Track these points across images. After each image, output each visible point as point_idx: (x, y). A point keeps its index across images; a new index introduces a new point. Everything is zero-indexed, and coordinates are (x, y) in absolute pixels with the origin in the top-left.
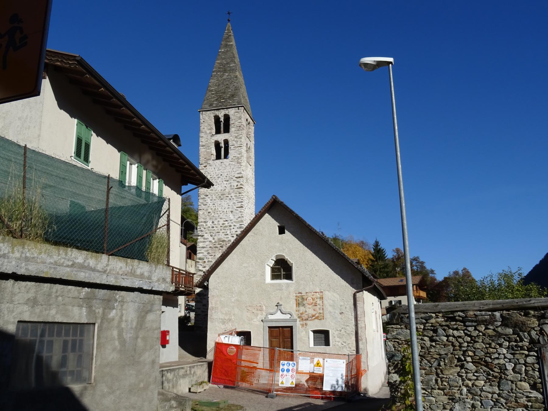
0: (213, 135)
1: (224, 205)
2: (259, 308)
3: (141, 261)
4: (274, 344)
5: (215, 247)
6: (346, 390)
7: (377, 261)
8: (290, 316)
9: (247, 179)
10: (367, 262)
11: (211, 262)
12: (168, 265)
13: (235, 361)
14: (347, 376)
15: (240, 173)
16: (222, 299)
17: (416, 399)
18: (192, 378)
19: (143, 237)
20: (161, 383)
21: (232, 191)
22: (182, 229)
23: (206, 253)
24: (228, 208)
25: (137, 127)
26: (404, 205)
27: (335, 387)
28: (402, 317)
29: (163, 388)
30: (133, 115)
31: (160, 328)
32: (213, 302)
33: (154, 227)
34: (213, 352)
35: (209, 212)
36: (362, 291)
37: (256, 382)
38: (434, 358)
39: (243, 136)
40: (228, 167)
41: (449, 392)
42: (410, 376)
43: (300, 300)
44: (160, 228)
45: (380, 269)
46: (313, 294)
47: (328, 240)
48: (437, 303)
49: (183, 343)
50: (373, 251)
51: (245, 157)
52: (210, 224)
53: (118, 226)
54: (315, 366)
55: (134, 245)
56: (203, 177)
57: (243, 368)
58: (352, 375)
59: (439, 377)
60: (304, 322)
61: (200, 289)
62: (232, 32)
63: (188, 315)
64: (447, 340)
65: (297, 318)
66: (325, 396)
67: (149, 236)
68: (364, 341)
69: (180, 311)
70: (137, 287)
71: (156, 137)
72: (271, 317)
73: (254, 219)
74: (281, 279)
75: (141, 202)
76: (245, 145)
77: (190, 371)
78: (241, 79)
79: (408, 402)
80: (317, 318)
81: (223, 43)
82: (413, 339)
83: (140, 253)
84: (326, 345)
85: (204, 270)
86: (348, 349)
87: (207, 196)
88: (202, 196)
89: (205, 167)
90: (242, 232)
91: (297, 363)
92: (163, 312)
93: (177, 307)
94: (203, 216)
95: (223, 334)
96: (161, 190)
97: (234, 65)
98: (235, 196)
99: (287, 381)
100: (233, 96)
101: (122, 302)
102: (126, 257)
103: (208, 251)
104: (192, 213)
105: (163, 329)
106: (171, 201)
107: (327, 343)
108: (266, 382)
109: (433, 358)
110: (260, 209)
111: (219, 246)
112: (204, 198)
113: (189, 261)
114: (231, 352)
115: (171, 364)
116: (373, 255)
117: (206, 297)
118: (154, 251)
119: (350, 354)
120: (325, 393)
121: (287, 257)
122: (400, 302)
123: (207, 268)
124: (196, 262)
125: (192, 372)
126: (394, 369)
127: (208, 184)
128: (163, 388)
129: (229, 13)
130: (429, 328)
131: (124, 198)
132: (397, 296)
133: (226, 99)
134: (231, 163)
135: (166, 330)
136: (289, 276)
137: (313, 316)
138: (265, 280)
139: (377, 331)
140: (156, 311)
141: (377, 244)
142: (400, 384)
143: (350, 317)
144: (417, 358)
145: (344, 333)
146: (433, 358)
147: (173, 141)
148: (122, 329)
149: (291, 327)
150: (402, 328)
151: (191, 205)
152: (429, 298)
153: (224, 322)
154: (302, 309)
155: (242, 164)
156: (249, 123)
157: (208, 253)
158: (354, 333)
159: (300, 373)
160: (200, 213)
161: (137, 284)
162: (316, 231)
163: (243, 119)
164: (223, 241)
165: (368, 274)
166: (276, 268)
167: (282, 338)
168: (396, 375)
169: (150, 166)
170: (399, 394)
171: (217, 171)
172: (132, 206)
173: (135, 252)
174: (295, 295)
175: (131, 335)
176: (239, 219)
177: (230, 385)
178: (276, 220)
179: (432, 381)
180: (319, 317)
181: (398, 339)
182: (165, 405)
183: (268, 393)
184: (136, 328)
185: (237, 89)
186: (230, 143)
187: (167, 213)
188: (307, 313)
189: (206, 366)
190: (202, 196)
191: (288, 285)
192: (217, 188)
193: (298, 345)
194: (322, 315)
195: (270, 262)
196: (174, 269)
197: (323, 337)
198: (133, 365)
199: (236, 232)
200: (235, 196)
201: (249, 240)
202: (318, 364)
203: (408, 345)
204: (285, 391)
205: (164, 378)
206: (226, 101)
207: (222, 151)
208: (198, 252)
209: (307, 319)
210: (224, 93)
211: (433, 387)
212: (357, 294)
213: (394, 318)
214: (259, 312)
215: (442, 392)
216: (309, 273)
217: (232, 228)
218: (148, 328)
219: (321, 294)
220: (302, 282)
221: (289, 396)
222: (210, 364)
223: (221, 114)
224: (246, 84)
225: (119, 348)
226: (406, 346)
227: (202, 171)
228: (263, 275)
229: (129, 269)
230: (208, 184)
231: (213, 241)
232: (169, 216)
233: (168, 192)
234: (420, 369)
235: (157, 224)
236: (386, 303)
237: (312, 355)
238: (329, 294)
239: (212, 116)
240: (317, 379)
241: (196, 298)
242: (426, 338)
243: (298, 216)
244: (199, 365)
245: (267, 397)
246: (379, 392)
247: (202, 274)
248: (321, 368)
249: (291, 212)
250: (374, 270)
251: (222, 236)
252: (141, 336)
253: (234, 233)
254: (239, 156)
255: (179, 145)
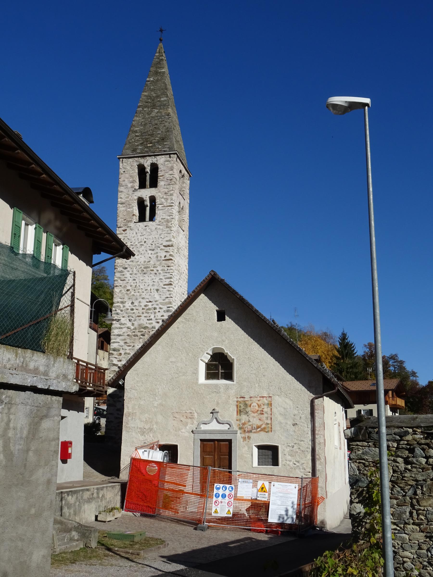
0: (135, 190)
1: (147, 281)
2: (189, 415)
3: (35, 352)
4: (208, 462)
5: (134, 336)
6: (297, 522)
7: (343, 358)
8: (229, 426)
9: (178, 249)
10: (331, 359)
11: (129, 354)
12: (71, 357)
13: (155, 482)
14: (299, 505)
15: (170, 241)
16: (142, 403)
17: (384, 537)
18: (100, 503)
19: (38, 320)
20: (60, 509)
21: (158, 263)
22: (91, 311)
23: (122, 343)
24: (153, 285)
25: (36, 177)
26: (377, 289)
27: (283, 518)
28: (370, 432)
29: (61, 515)
30: (31, 161)
31: (58, 439)
32: (130, 406)
33: (54, 308)
34: (128, 470)
35: (128, 290)
36: (322, 397)
37: (182, 510)
38: (410, 485)
39: (175, 192)
40: (155, 232)
41: (426, 528)
42: (377, 507)
43: (242, 407)
44: (61, 309)
45: (347, 368)
46: (259, 399)
47: (280, 331)
48: (415, 416)
49: (89, 458)
50: (338, 346)
51: (177, 219)
52: (128, 305)
53: (6, 305)
54: (258, 491)
55: (26, 331)
56: (121, 245)
57: (166, 492)
58: (305, 504)
59: (414, 509)
60: (247, 434)
61: (114, 389)
62: (164, 55)
63: (97, 422)
64: (426, 463)
65: (237, 429)
66: (271, 529)
67: (48, 320)
68: (323, 460)
69: (87, 416)
70: (29, 385)
71: (61, 190)
72: (203, 427)
73: (185, 301)
74: (218, 379)
75: (37, 276)
76: (177, 204)
77: (98, 493)
78: (174, 117)
79: (373, 540)
80: (263, 430)
81: (152, 69)
82: (383, 461)
83: (34, 341)
84: (273, 465)
85: (120, 364)
86: (302, 471)
87: (126, 268)
88: (120, 269)
89: (124, 231)
90: (170, 317)
91: (236, 486)
92: (63, 418)
93: (83, 412)
94: (120, 295)
95: (142, 447)
96: (65, 260)
97: (165, 99)
98: (162, 270)
99: (222, 510)
100: (163, 139)
101: (10, 404)
102: (16, 347)
103: (125, 340)
104: (107, 290)
105: (63, 438)
106: (76, 275)
107: (275, 462)
108: (196, 510)
109: (407, 484)
110: (193, 288)
111: (139, 334)
112: (121, 272)
113: (100, 352)
114: (151, 471)
115: (73, 484)
116: (338, 351)
117: (120, 399)
118: (53, 339)
119: (304, 476)
120: (271, 525)
121: (227, 351)
122: (370, 412)
123: (124, 362)
124: (110, 354)
125: (100, 496)
126: (358, 497)
127: (128, 254)
128: (61, 515)
129: (161, 31)
130: (404, 446)
131: (16, 269)
132: (368, 404)
133: (154, 142)
134: (159, 227)
135: (67, 440)
136: (229, 376)
137: (258, 427)
138: (197, 379)
139: (340, 449)
140: (53, 416)
141: (344, 337)
142: (364, 517)
143: (306, 429)
144: (387, 484)
145: (297, 450)
146: (407, 484)
147: (84, 196)
148: (9, 439)
149: (230, 441)
150: (369, 446)
151: (106, 279)
152: (409, 407)
153: (143, 432)
154: (244, 418)
155: (172, 229)
156: (183, 176)
157: (126, 343)
158: (310, 450)
159: (240, 500)
160: (116, 290)
161: (29, 381)
162: (265, 318)
163: (175, 170)
164: (145, 328)
165: (330, 375)
166: (212, 365)
167: (218, 455)
168: (359, 505)
169: (51, 228)
170: (363, 529)
171: (139, 237)
172: (25, 280)
173: (27, 340)
174: (236, 399)
175: (21, 447)
176: (167, 300)
177: (149, 513)
178: (215, 302)
179: (405, 514)
180: (266, 429)
181: (364, 459)
182: (64, 537)
183: (197, 524)
184: (27, 438)
185: (169, 130)
186: (158, 201)
187: (71, 290)
188: (250, 423)
189: (118, 487)
190: (120, 269)
191: (227, 387)
192: (139, 258)
193: (238, 464)
194: (270, 426)
195: (205, 357)
196: (80, 363)
197: (270, 454)
198: (22, 484)
199: (162, 316)
200: (162, 270)
201: (178, 328)
202: (262, 488)
203: (377, 467)
204: (219, 521)
205: (63, 502)
206: (154, 145)
207: (147, 211)
208: (112, 341)
209: (251, 431)
210: (152, 135)
211: (407, 521)
212: (316, 400)
213: (360, 432)
214: (189, 421)
215: (418, 528)
216: (254, 372)
217: (157, 311)
218: (43, 438)
219: (270, 399)
220: (245, 383)
221: (224, 529)
222: (123, 486)
223: (147, 163)
224: (181, 125)
225: (4, 463)
226: (374, 469)
227: (120, 236)
228: (196, 372)
229: (18, 361)
230: (128, 254)
231: (132, 327)
232: (73, 294)
233: (75, 263)
234: (391, 498)
235: (58, 304)
236: (352, 413)
237: (254, 476)
238: (280, 399)
239: (135, 165)
240: (260, 508)
241: (108, 400)
242: (400, 460)
243: (243, 299)
244: (110, 487)
245: (195, 529)
246: (340, 525)
247: (117, 369)
248: (267, 494)
249: (234, 293)
250: (339, 370)
251: (144, 321)
252: (33, 448)
253: (160, 317)
254: (169, 218)
255: (91, 202)
